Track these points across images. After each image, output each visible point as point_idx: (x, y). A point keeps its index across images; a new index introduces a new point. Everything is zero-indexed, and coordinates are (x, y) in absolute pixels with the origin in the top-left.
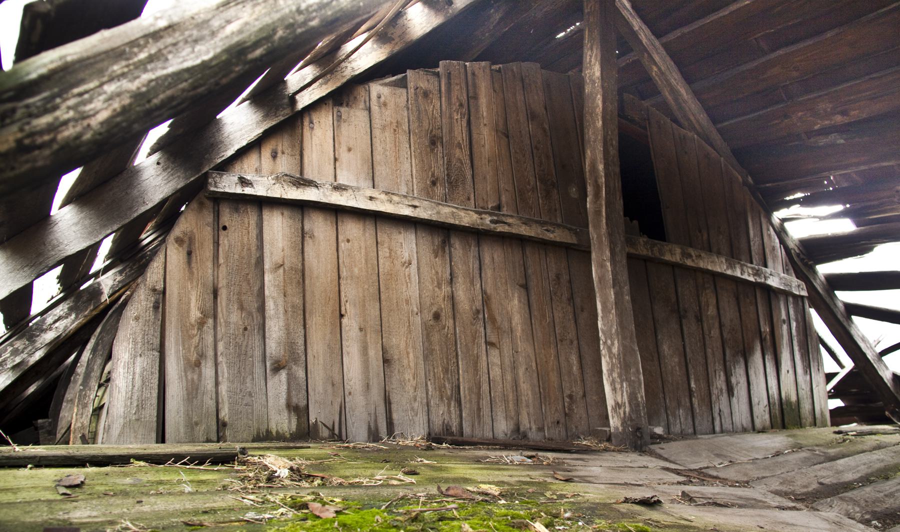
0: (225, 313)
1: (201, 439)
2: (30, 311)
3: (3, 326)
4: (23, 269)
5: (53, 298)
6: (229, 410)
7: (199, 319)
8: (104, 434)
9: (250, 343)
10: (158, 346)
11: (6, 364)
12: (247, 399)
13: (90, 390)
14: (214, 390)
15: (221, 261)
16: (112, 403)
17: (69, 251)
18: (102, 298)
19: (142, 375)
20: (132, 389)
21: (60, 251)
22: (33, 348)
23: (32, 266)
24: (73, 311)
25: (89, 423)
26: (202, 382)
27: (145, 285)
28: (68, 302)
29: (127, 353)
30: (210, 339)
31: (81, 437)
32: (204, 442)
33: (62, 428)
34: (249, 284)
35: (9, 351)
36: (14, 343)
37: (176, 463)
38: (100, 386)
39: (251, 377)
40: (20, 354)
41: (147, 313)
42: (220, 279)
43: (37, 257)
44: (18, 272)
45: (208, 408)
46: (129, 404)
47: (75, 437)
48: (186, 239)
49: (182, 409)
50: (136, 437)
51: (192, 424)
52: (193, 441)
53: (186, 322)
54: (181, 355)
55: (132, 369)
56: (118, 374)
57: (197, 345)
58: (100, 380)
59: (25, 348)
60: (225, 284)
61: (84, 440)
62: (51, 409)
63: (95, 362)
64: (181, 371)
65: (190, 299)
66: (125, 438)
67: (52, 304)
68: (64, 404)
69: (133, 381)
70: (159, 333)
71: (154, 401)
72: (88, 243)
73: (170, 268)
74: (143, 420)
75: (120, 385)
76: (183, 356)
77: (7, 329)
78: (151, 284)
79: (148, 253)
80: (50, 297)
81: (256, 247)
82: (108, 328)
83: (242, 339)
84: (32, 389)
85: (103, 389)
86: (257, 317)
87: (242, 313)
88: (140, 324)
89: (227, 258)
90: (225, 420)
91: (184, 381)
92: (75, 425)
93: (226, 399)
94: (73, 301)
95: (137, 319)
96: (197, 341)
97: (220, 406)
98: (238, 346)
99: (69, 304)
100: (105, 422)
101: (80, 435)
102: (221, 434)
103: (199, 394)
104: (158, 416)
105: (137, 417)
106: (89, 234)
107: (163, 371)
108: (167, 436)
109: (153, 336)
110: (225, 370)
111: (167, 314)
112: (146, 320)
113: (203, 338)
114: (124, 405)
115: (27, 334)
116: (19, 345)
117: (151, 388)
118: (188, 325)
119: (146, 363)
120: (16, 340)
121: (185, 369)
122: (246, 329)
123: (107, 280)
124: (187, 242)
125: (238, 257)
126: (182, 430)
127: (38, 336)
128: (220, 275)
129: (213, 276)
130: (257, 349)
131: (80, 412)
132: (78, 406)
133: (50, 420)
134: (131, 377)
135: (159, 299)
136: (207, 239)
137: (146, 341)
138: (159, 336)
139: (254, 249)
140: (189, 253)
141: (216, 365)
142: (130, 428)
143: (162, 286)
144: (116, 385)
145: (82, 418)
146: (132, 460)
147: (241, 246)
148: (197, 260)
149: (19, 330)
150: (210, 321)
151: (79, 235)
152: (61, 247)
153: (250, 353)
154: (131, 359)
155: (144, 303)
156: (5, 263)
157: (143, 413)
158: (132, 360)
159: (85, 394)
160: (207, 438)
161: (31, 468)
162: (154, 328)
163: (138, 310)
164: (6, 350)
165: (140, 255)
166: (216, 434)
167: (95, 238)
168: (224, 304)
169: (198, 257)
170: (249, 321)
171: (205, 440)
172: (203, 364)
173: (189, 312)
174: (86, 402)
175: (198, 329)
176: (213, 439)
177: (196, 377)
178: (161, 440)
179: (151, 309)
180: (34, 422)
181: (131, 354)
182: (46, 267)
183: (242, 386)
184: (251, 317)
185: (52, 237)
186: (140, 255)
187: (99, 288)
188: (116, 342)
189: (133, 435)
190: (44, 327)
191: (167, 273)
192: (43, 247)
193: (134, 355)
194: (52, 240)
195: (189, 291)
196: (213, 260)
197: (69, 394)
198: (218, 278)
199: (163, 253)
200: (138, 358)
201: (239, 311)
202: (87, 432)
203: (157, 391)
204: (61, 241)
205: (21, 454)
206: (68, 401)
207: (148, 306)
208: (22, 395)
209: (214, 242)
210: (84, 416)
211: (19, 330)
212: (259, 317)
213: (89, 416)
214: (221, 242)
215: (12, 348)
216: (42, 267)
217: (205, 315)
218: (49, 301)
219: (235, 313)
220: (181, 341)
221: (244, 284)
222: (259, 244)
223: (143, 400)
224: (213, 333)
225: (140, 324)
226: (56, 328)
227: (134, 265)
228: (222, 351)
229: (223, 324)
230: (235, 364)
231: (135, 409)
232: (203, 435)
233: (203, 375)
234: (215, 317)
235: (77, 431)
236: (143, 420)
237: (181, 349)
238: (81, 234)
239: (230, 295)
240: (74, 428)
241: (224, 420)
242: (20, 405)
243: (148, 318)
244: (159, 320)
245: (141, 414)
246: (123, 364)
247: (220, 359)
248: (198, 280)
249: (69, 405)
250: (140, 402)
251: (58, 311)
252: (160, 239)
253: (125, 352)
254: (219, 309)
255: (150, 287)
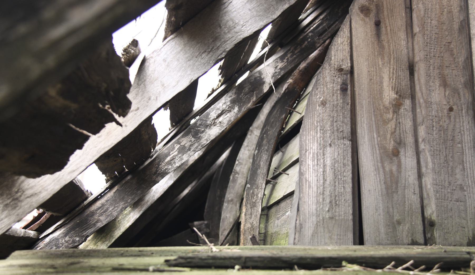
0: (424, 91)
1: (406, 241)
2: (192, 105)
3: (169, 122)
4: (201, 55)
5: (213, 91)
6: (437, 206)
7: (394, 100)
8: (295, 234)
9: (457, 126)
10: (349, 134)
11: (175, 163)
12: (458, 194)
13: (257, 188)
14: (417, 183)
15: (416, 29)
16: (302, 199)
17: (246, 32)
18: (264, 88)
19: (333, 166)
20: (324, 183)
21: (237, 33)
22: (199, 145)
23: (210, 52)
24: (236, 104)
25: (258, 224)
26: (403, 174)
27: (330, 65)
28: (230, 94)
29: (316, 143)
30: (408, 124)
31: (251, 239)
32: (409, 245)
33: (225, 230)
34: (452, 55)
35: (176, 149)
36: (181, 140)
37: (397, 268)
38: (268, 182)
39: (461, 167)
40: (187, 152)
41: (335, 97)
42: (416, 51)
43: (213, 41)
44: (196, 59)
45: (411, 204)
46: (321, 200)
47: (245, 239)
48: (373, 7)
49: (381, 205)
50: (330, 238)
51: (393, 223)
52: (396, 243)
53: (379, 105)
54: (376, 143)
55: (322, 161)
56: (307, 166)
57: (393, 130)
58: (267, 177)
59: (191, 145)
60: (422, 57)
61: (254, 241)
62: (205, 211)
63: (261, 158)
64: (377, 162)
65: (381, 78)
66: (319, 238)
67: (214, 98)
68: (225, 204)
69: (324, 175)
70: (349, 119)
71: (349, 197)
72: (265, 22)
73: (357, 43)
74: (337, 218)
75: (310, 179)
76: (378, 144)
77: (172, 126)
78: (336, 63)
79: (310, 34)
80: (211, 90)
81: (459, 9)
82: (272, 120)
83: (447, 121)
84: (186, 191)
85: (270, 186)
86: (464, 95)
87: (445, 91)
88: (328, 110)
89: (423, 26)
90: (433, 218)
91: (381, 172)
92: (245, 225)
93: (432, 194)
94: (235, 93)
95: (323, 104)
96: (394, 127)
97: (426, 202)
98: (442, 130)
99: (231, 96)
100: (296, 220)
101: (250, 237)
102: (429, 235)
103: (399, 188)
104: (354, 214)
105: (331, 215)
106: (265, 11)
107: (356, 162)
108: (366, 237)
109: (343, 122)
110: (429, 159)
111: (357, 97)
112: (334, 105)
113: (399, 123)
114: (315, 201)
115: (192, 130)
116: (186, 141)
117: (345, 182)
118: (382, 108)
119: (336, 154)
120: (183, 136)
121: (381, 159)
122: (451, 109)
123: (268, 68)
124: (374, 11)
125: (436, 22)
126: (383, 230)
127: (203, 132)
128: (416, 47)
129: (407, 48)
130: (467, 133)
131: (249, 212)
132: (246, 205)
133: (206, 222)
134: (321, 170)
135: (346, 79)
136: (397, 5)
137: (335, 128)
138: (349, 123)
139: (456, 10)
140: (378, 24)
141: (418, 153)
142: (324, 227)
143: (349, 65)
144: (306, 179)
145: (251, 218)
146: (344, 263)
147: (440, 8)
148: (386, 30)
149: (184, 127)
150: (408, 103)
151: (255, 13)
152: (238, 28)
153: (458, 138)
154: (320, 149)
155: (330, 86)
156: (183, 51)
157: (337, 210)
158: (321, 151)
159: (253, 193)
160: (412, 240)
161: (239, 270)
162: (343, 114)
163: (324, 93)
164: (174, 148)
165: (301, 37)
166: (422, 236)
167: (272, 15)
168: (423, 81)
169: (388, 28)
170: (455, 100)
171: (410, 242)
172: (402, 153)
173: (382, 93)
174: (254, 201)
175: (394, 112)
176: (419, 241)
177: (394, 168)
178: (358, 241)
179: (339, 92)
180: (190, 224)
181: (320, 144)
182: (224, 52)
183: (450, 178)
184: (456, 95)
185: (226, 18)
186: (301, 37)
187: (260, 77)
188: (303, 131)
189: (327, 235)
190: (208, 122)
191: (354, 49)
192: (219, 30)
193: (324, 145)
194: (228, 21)
195: (380, 69)
196: (407, 30)
197: (230, 193)
198: (413, 50)
199: (348, 26)
200: (328, 148)
201: (442, 89)
202: (257, 233)
203: (351, 185)
204: (237, 21)
205: (218, 255)
206: (229, 202)
207: (335, 89)
208: (179, 197)
209: (406, 8)
210: (253, 216)
211: (184, 127)
212: (467, 95)
213: (259, 216)
214: (414, 7)
215: (179, 146)
216: (219, 52)
217: (401, 96)
218: (209, 95)
219: (437, 92)
220: (374, 127)
221: (447, 56)
222: (463, 4)
223: (336, 196)
224: (411, 117)
225: (328, 110)
226: (220, 122)
227: (295, 49)
228: (424, 137)
229: (423, 105)
230: (440, 151)
231: (328, 206)
232: (407, 236)
233: (403, 166)
234: (413, 97)
235: (247, 233)
236: (337, 218)
237: (375, 136)
238: (257, 11)
239: (429, 69)
240: (244, 229)
241: (431, 218)
242: (178, 206)
243: (336, 103)
244: (348, 104)
245: (336, 212)
246: (311, 155)
247: (422, 146)
248: (390, 54)
249: (230, 206)
250: (333, 198)
251: (221, 104)
252: (321, 17)
253: (314, 142)
254: (417, 88)
255: (336, 66)
